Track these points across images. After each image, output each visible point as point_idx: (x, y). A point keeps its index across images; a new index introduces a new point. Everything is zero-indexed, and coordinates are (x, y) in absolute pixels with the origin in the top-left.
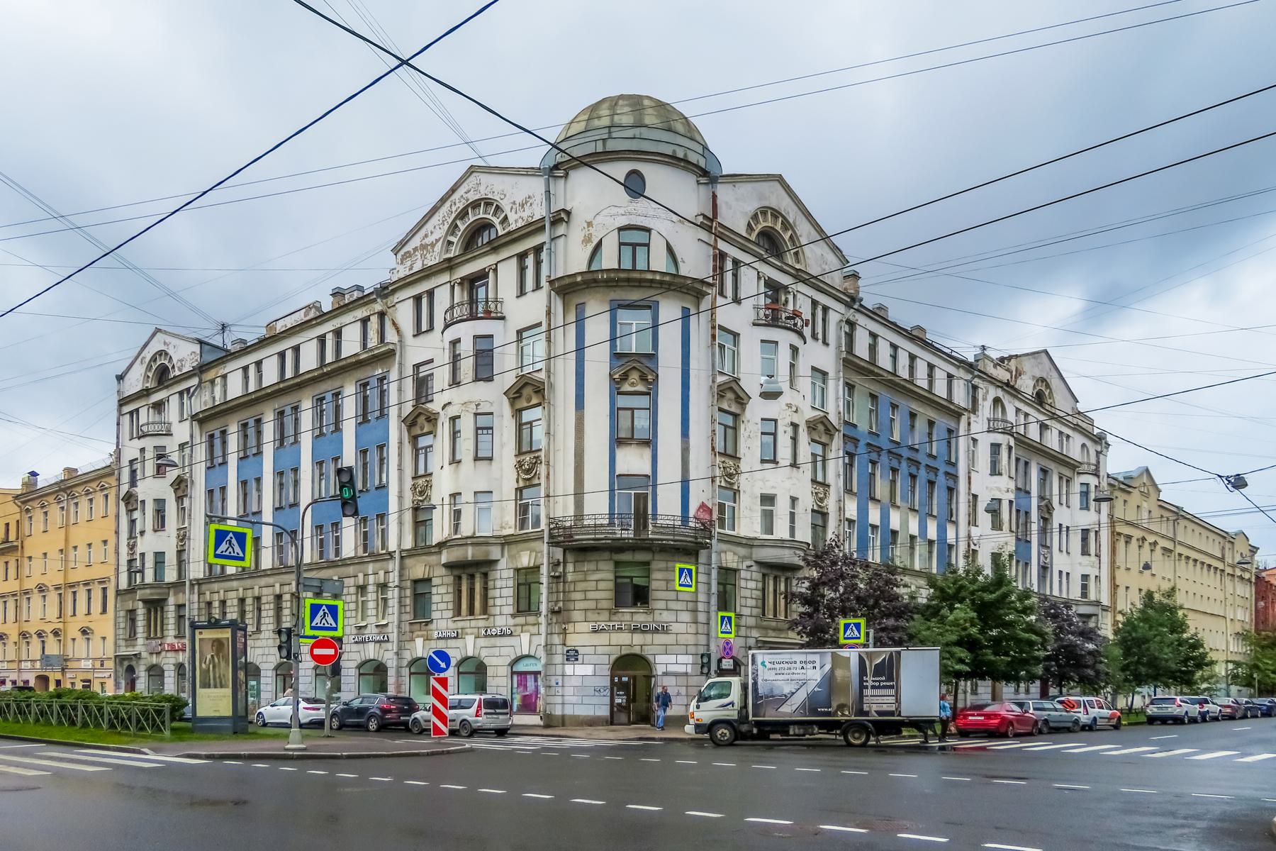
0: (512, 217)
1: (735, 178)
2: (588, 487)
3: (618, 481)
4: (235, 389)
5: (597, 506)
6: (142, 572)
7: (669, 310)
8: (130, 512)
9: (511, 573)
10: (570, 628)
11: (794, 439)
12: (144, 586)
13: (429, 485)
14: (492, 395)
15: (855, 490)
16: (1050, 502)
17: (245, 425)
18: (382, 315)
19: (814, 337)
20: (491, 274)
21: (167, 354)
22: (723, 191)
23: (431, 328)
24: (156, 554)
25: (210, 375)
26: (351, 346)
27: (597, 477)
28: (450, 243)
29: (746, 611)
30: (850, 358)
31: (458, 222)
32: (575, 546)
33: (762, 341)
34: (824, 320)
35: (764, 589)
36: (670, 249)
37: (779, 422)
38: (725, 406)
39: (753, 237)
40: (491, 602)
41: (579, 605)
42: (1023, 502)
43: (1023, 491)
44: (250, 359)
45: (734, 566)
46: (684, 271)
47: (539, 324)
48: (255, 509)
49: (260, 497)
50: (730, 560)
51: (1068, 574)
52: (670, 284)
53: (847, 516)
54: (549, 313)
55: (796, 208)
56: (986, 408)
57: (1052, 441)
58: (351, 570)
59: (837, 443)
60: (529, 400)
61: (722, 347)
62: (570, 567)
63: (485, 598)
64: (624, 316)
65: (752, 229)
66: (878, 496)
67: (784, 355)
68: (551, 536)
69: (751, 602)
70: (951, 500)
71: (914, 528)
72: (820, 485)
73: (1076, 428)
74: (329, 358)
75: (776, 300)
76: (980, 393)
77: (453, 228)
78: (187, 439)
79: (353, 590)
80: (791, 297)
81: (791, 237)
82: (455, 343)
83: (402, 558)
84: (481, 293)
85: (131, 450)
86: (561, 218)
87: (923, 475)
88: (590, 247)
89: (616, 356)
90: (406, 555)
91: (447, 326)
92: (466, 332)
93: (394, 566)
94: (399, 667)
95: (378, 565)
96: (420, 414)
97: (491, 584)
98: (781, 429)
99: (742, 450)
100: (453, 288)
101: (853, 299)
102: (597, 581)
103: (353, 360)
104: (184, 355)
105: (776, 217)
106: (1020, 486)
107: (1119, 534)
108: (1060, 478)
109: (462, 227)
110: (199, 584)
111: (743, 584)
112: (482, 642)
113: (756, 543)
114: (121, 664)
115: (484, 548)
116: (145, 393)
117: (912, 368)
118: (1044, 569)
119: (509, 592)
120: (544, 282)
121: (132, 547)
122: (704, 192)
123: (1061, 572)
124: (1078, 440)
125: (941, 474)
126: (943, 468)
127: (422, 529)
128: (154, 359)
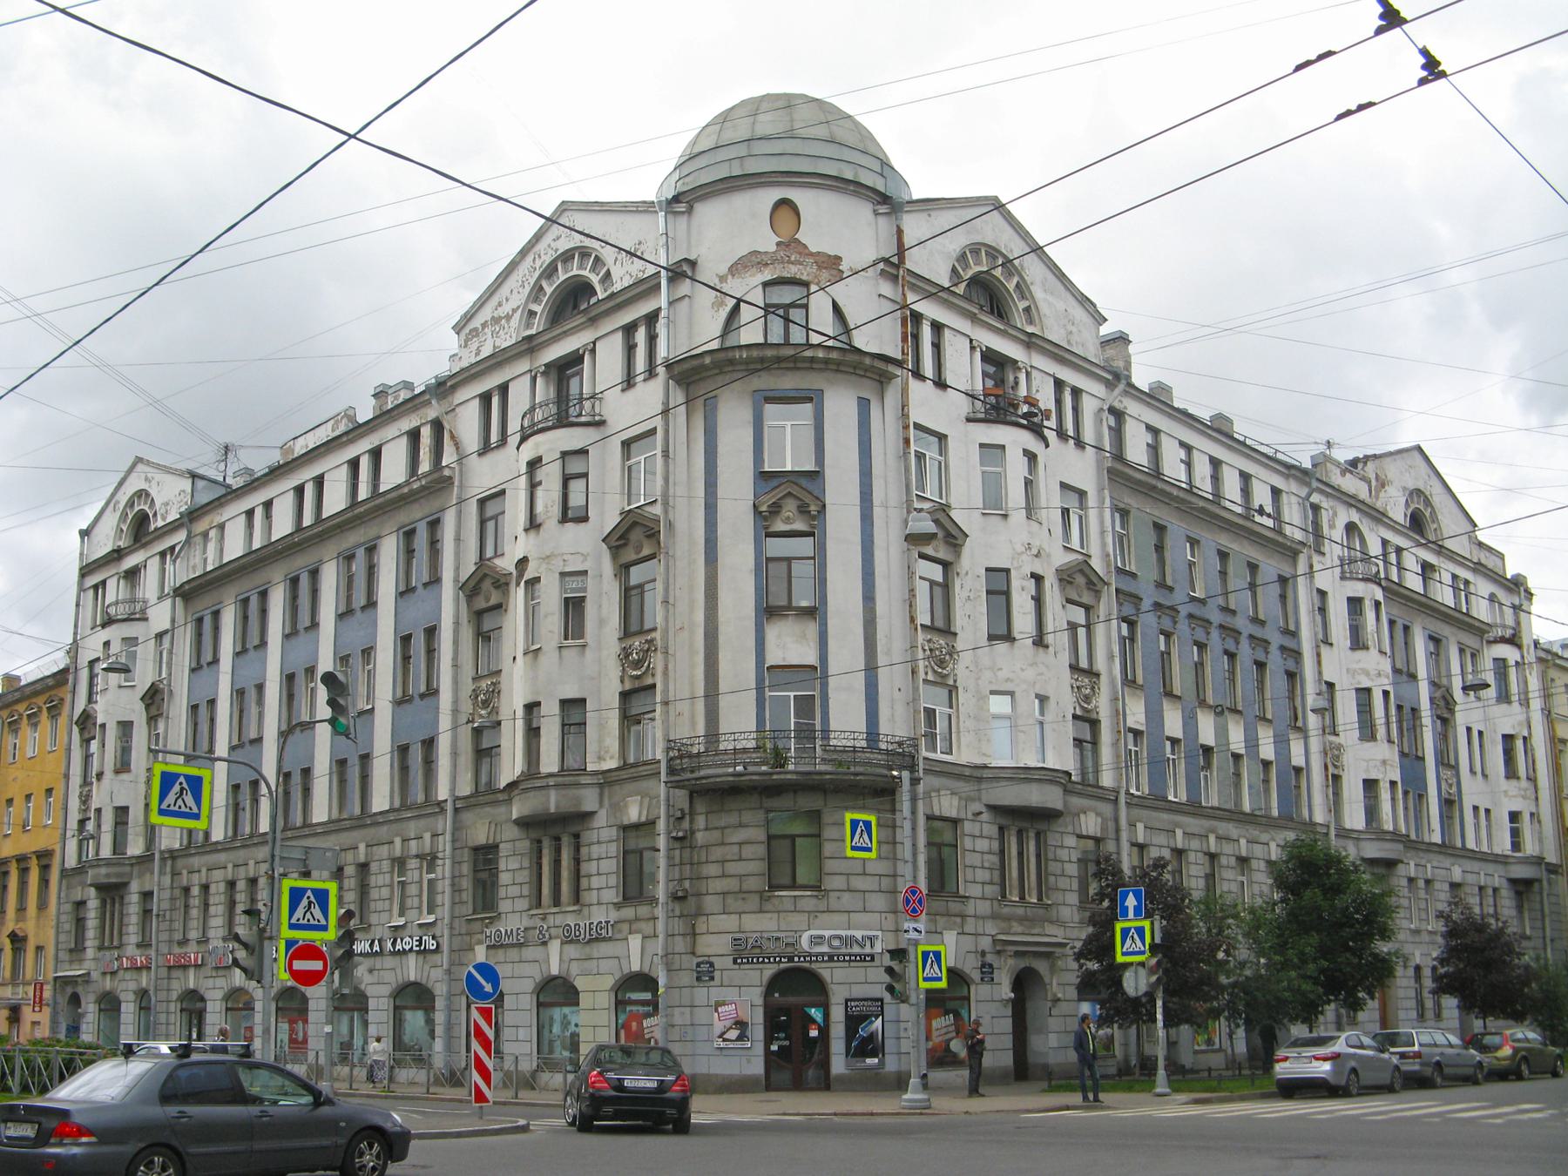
0: (616, 273)
1: (929, 204)
2: (882, 660)
3: (771, 675)
4: (234, 548)
6: (96, 837)
7: (840, 404)
8: (86, 742)
9: (614, 832)
10: (701, 927)
11: (1038, 600)
12: (98, 862)
13: (495, 691)
14: (583, 546)
15: (1140, 680)
16: (1449, 691)
17: (246, 601)
18: (438, 426)
20: (587, 358)
21: (148, 495)
22: (915, 228)
24: (117, 809)
25: (200, 526)
26: (394, 472)
27: (738, 669)
28: (532, 314)
29: (975, 890)
30: (1119, 466)
31: (544, 284)
32: (709, 788)
33: (982, 446)
34: (1076, 409)
35: (1002, 852)
36: (836, 309)
39: (960, 289)
40: (584, 883)
41: (718, 885)
42: (1406, 689)
43: (1405, 674)
44: (255, 500)
45: (953, 814)
46: (861, 341)
47: (653, 432)
48: (253, 735)
49: (261, 715)
50: (948, 806)
51: (1487, 811)
52: (839, 363)
53: (1131, 723)
57: (1445, 596)
59: (1107, 604)
60: (639, 549)
62: (701, 821)
63: (577, 876)
66: (1177, 692)
67: (1016, 467)
68: (672, 771)
70: (1292, 691)
72: (1084, 673)
73: (1479, 568)
74: (363, 493)
75: (1000, 382)
76: (1325, 517)
77: (538, 290)
78: (167, 626)
79: (386, 865)
80: (1022, 377)
81: (1018, 286)
83: (456, 810)
84: (574, 383)
85: (92, 647)
87: (1245, 652)
88: (724, 313)
89: (764, 477)
90: (463, 806)
91: (523, 439)
93: (446, 823)
94: (450, 996)
95: (422, 823)
97: (584, 851)
98: (1016, 584)
99: (959, 622)
100: (534, 379)
101: (1117, 376)
102: (741, 840)
103: (394, 495)
104: (170, 498)
105: (995, 258)
106: (1399, 666)
108: (1462, 651)
109: (549, 290)
110: (174, 858)
112: (573, 951)
114: (63, 989)
115: (572, 792)
116: (117, 555)
117: (1216, 478)
118: (1449, 804)
119: (610, 865)
120: (661, 370)
121: (85, 799)
122: (885, 226)
123: (1476, 808)
124: (1483, 587)
125: (1274, 649)
126: (1276, 639)
127: (486, 762)
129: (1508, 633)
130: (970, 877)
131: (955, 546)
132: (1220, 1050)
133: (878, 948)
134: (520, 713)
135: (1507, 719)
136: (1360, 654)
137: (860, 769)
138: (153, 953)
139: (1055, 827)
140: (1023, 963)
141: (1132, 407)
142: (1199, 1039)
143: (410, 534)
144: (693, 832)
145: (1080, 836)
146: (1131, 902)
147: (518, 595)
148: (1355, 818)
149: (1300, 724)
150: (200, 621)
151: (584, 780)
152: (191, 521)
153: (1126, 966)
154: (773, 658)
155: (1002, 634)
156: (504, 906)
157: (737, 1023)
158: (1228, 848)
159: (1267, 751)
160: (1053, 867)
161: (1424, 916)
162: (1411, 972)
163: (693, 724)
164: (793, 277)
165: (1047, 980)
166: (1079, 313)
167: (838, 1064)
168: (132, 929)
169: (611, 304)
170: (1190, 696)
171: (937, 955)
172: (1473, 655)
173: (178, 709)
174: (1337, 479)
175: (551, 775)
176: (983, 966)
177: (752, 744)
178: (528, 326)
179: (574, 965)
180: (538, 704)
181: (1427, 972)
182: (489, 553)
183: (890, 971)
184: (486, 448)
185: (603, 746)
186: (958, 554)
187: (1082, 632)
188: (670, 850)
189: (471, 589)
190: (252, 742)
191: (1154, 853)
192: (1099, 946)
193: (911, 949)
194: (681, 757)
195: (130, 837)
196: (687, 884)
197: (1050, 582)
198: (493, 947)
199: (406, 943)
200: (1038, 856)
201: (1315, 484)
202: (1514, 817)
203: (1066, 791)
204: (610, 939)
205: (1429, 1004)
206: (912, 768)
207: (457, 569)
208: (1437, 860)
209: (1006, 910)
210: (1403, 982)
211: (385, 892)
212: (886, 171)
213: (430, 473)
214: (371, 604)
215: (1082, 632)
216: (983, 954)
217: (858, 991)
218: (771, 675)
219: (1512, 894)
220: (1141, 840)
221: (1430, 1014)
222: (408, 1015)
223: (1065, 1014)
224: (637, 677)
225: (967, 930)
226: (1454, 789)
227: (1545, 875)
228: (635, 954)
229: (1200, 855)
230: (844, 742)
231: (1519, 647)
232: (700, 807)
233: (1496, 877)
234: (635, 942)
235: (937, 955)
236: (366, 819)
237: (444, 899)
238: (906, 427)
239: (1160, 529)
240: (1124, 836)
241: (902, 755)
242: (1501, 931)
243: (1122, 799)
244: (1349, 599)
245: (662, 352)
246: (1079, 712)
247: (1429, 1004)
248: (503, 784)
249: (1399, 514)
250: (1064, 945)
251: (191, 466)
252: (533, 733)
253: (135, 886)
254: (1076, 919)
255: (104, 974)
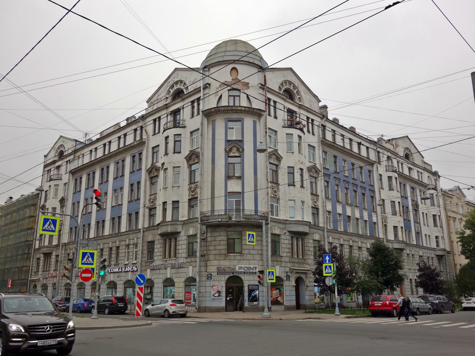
3: (229, 194)
4: (87, 160)
5: (220, 207)
7: (248, 122)
9: (186, 237)
10: (208, 264)
11: (302, 175)
12: (44, 247)
13: (155, 199)
14: (180, 159)
15: (330, 198)
16: (417, 202)
17: (89, 175)
18: (142, 127)
19: (308, 131)
21: (63, 146)
22: (269, 75)
23: (159, 132)
25: (78, 154)
26: (130, 140)
27: (220, 192)
29: (284, 254)
31: (170, 90)
32: (212, 226)
33: (287, 134)
35: (292, 244)
37: (295, 168)
38: (272, 162)
39: (282, 92)
40: (177, 251)
41: (213, 252)
43: (404, 197)
44: (92, 147)
47: (198, 129)
48: (89, 211)
50: (277, 231)
51: (429, 236)
52: (248, 111)
53: (327, 209)
54: (202, 124)
55: (298, 80)
56: (384, 162)
57: (415, 175)
58: (124, 237)
60: (194, 161)
61: (270, 136)
62: (209, 234)
64: (230, 124)
65: (281, 89)
66: (340, 201)
67: (296, 139)
68: (201, 220)
69: (287, 250)
70: (373, 201)
71: (357, 215)
72: (314, 195)
73: (425, 169)
75: (292, 117)
78: (67, 181)
79: (124, 247)
81: (297, 92)
82: (167, 138)
83: (144, 231)
84: (178, 117)
86: (207, 86)
87: (359, 191)
89: (228, 141)
90: (146, 230)
91: (164, 131)
92: (172, 132)
95: (134, 235)
96: (153, 168)
97: (178, 242)
98: (296, 171)
99: (280, 181)
101: (324, 116)
102: (220, 240)
104: (69, 147)
105: (291, 84)
106: (403, 195)
107: (450, 217)
108: (420, 191)
110: (65, 245)
111: (283, 241)
112: (174, 271)
113: (288, 222)
115: (175, 226)
116: (54, 162)
118: (418, 234)
119: (185, 247)
120: (201, 113)
123: (426, 235)
124: (426, 175)
126: (368, 188)
127: (152, 218)
128: (59, 148)
129: (434, 187)
130: (283, 251)
131: (279, 160)
132: (355, 302)
133: (257, 270)
134: (161, 204)
135: (434, 211)
136: (391, 192)
137: (252, 220)
138: (58, 272)
139: (307, 237)
140: (298, 275)
141: (328, 125)
142: (349, 298)
143: (134, 157)
144: (207, 238)
145: (314, 240)
146: (327, 258)
147: (162, 173)
148: (391, 236)
149: (375, 210)
150: (76, 180)
151: (178, 223)
152: (75, 153)
153: (326, 277)
154: (229, 190)
155: (292, 184)
156: (155, 258)
157: (218, 291)
158: (355, 244)
159: (366, 218)
160: (306, 248)
161: (412, 265)
162: (409, 281)
163: (208, 207)
164: (234, 87)
165: (305, 280)
166: (314, 99)
167: (246, 304)
168: (52, 266)
169: (188, 95)
170: (344, 202)
171: (273, 272)
172: (424, 193)
173: (69, 204)
174: (384, 144)
175: (169, 222)
176: (287, 276)
177: (223, 213)
178: (166, 101)
179: (174, 275)
180: (166, 202)
181: (413, 281)
182: (155, 162)
183: (259, 277)
184: (155, 134)
185: (183, 214)
186: (280, 163)
187: (314, 184)
188: (201, 242)
189: (149, 171)
190: (89, 213)
191: (334, 244)
192: (319, 272)
193: (265, 271)
194: (204, 217)
195: (54, 240)
196: (205, 252)
197: (305, 170)
198: (152, 270)
199: (128, 269)
200: (302, 245)
201: (378, 146)
202: (437, 237)
203: (310, 227)
204: (184, 267)
205: (414, 290)
206: (267, 220)
207: (146, 166)
208: (415, 249)
209: (293, 260)
210: (406, 283)
211: (123, 254)
212: (262, 60)
213: (139, 140)
214: (123, 175)
215: (314, 184)
216: (287, 272)
217: (252, 283)
218: (229, 194)
219: (437, 259)
220: (331, 241)
221: (415, 293)
222: (128, 289)
223: (312, 292)
224: (193, 195)
225: (282, 265)
226: (419, 229)
227: (446, 254)
228: (190, 272)
229: (348, 246)
230: (248, 213)
231: (437, 191)
232: (209, 230)
233: (432, 254)
234: (191, 268)
235: (273, 272)
236: (119, 234)
237: (139, 256)
238: (266, 129)
239: (335, 157)
240: (326, 240)
241: (264, 216)
242: (435, 270)
243: (325, 230)
244: (388, 177)
245: (201, 107)
246: (313, 206)
247: (414, 290)
248: (157, 223)
249: (402, 154)
250: (309, 270)
251: (76, 139)
252: (165, 210)
253: (54, 254)
254: (313, 263)
255: (44, 279)
